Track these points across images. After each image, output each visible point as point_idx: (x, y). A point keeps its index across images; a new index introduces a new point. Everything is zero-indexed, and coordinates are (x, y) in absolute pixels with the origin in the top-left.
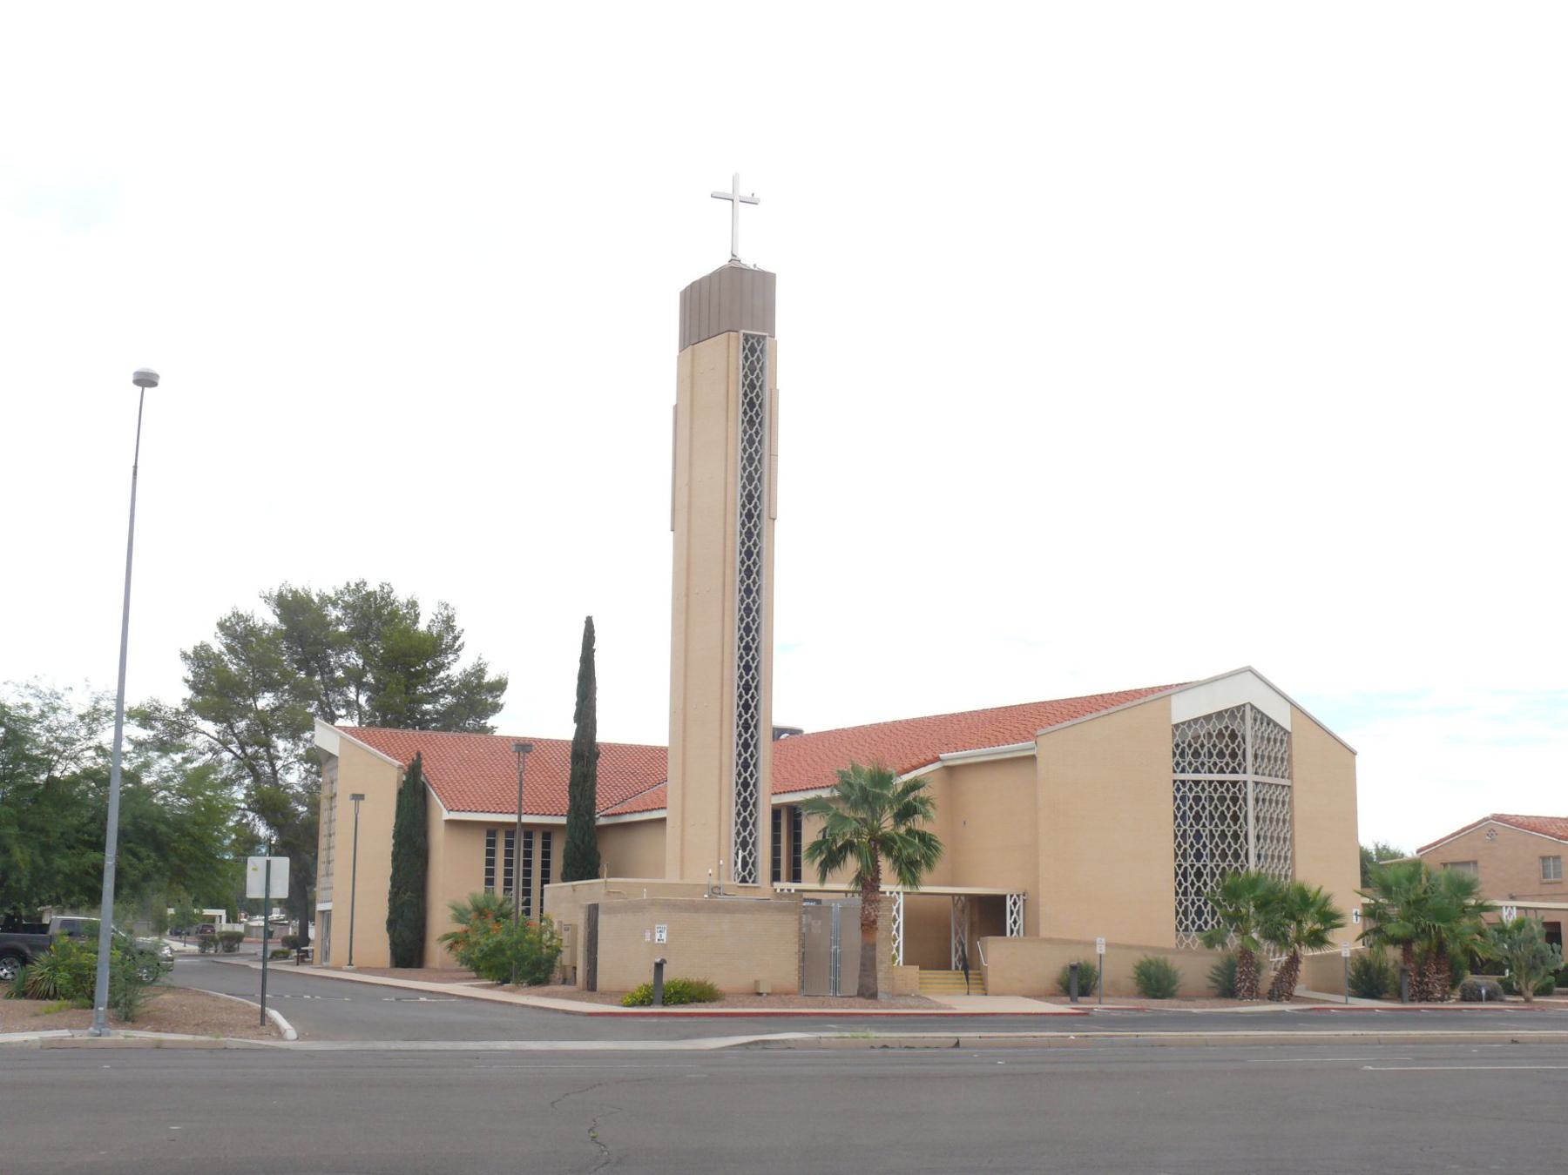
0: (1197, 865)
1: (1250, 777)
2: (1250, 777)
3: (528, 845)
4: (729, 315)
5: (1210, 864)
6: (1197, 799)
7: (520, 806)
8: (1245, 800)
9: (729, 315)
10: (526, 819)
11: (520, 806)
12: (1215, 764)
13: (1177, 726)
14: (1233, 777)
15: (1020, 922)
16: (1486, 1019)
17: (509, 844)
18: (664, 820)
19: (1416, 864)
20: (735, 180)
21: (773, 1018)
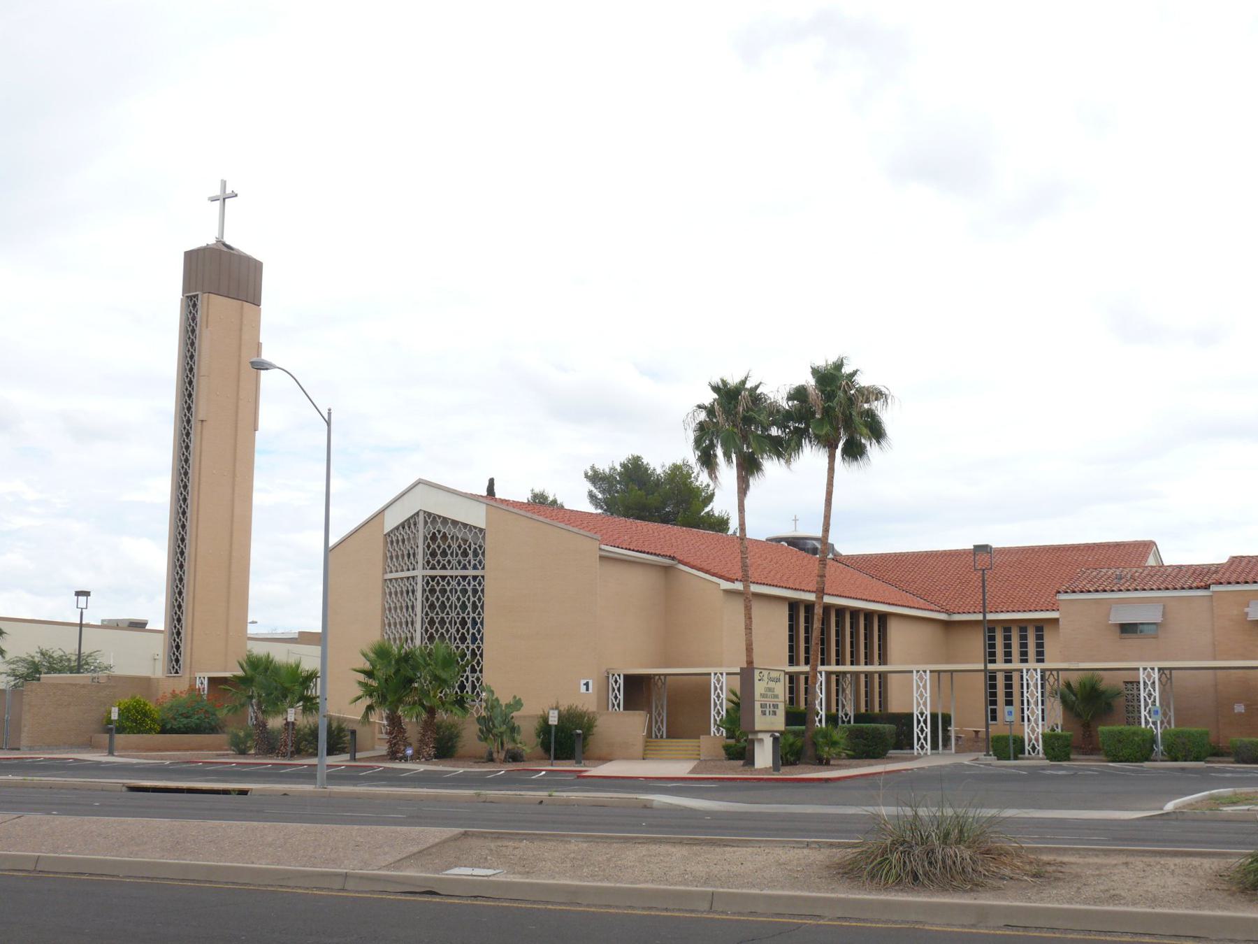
0: (462, 646)
1: (420, 573)
2: (420, 573)
3: (1024, 637)
4: (220, 280)
5: (471, 647)
6: (443, 591)
7: (984, 607)
8: (424, 591)
9: (220, 280)
10: (990, 617)
11: (984, 607)
12: (439, 562)
13: (388, 534)
14: (443, 573)
15: (611, 697)
16: (282, 775)
17: (1024, 637)
18: (1056, 621)
19: (1103, 693)
20: (213, 200)
21: (816, 784)
